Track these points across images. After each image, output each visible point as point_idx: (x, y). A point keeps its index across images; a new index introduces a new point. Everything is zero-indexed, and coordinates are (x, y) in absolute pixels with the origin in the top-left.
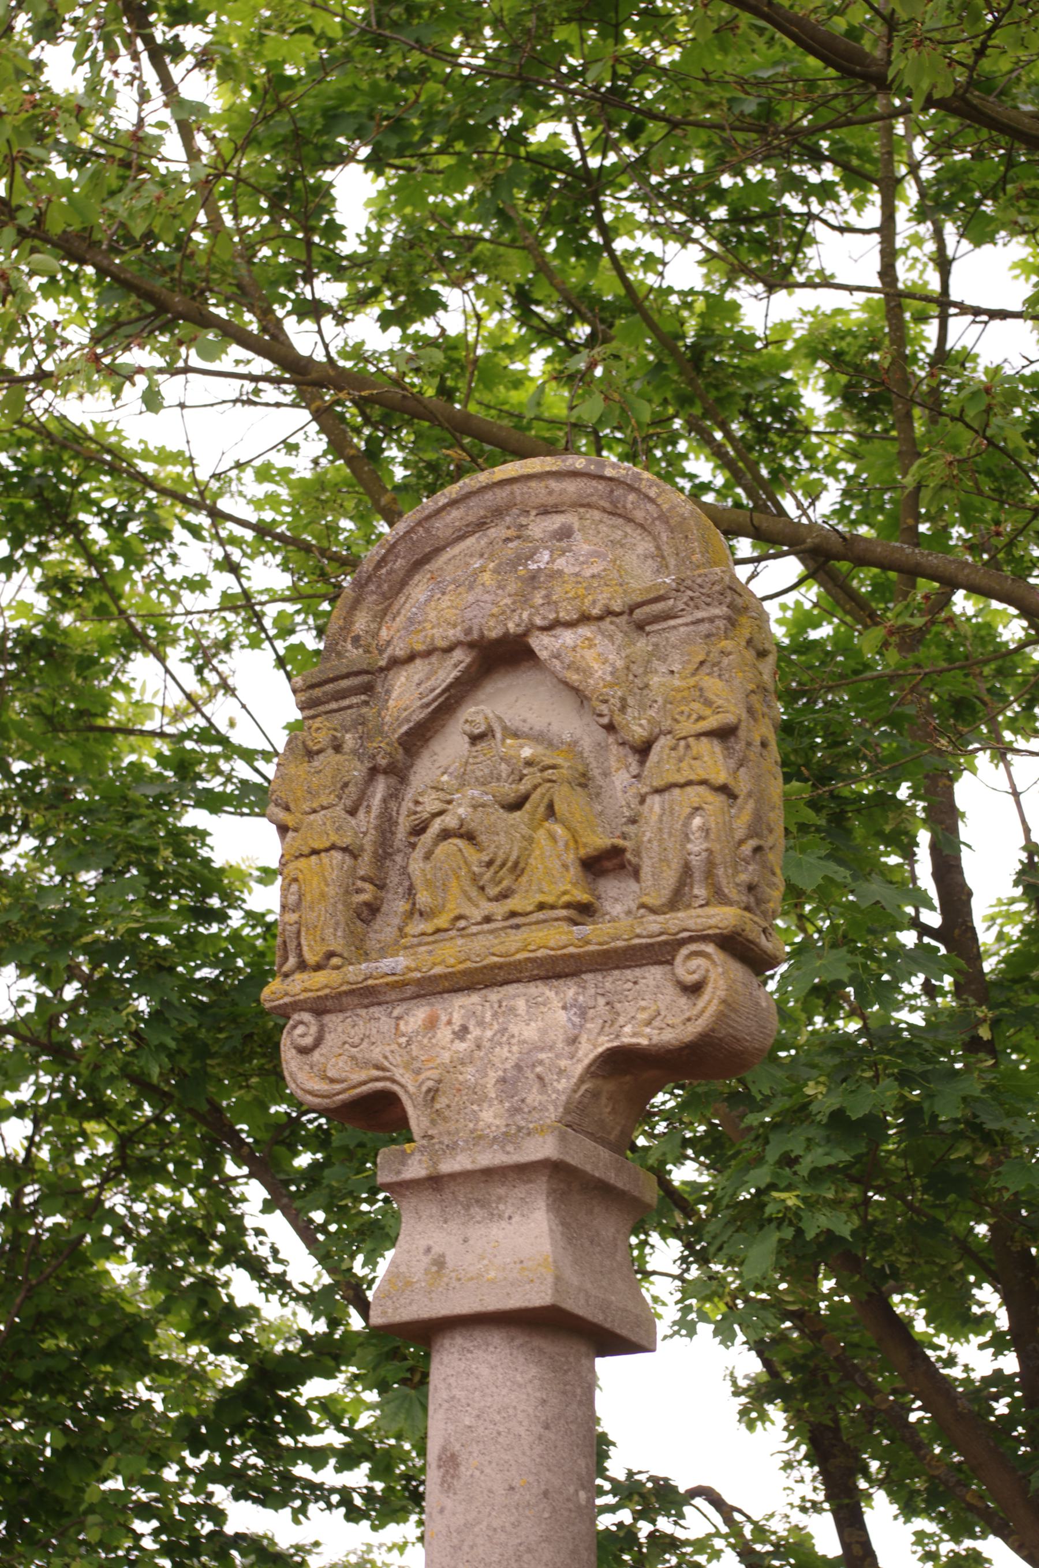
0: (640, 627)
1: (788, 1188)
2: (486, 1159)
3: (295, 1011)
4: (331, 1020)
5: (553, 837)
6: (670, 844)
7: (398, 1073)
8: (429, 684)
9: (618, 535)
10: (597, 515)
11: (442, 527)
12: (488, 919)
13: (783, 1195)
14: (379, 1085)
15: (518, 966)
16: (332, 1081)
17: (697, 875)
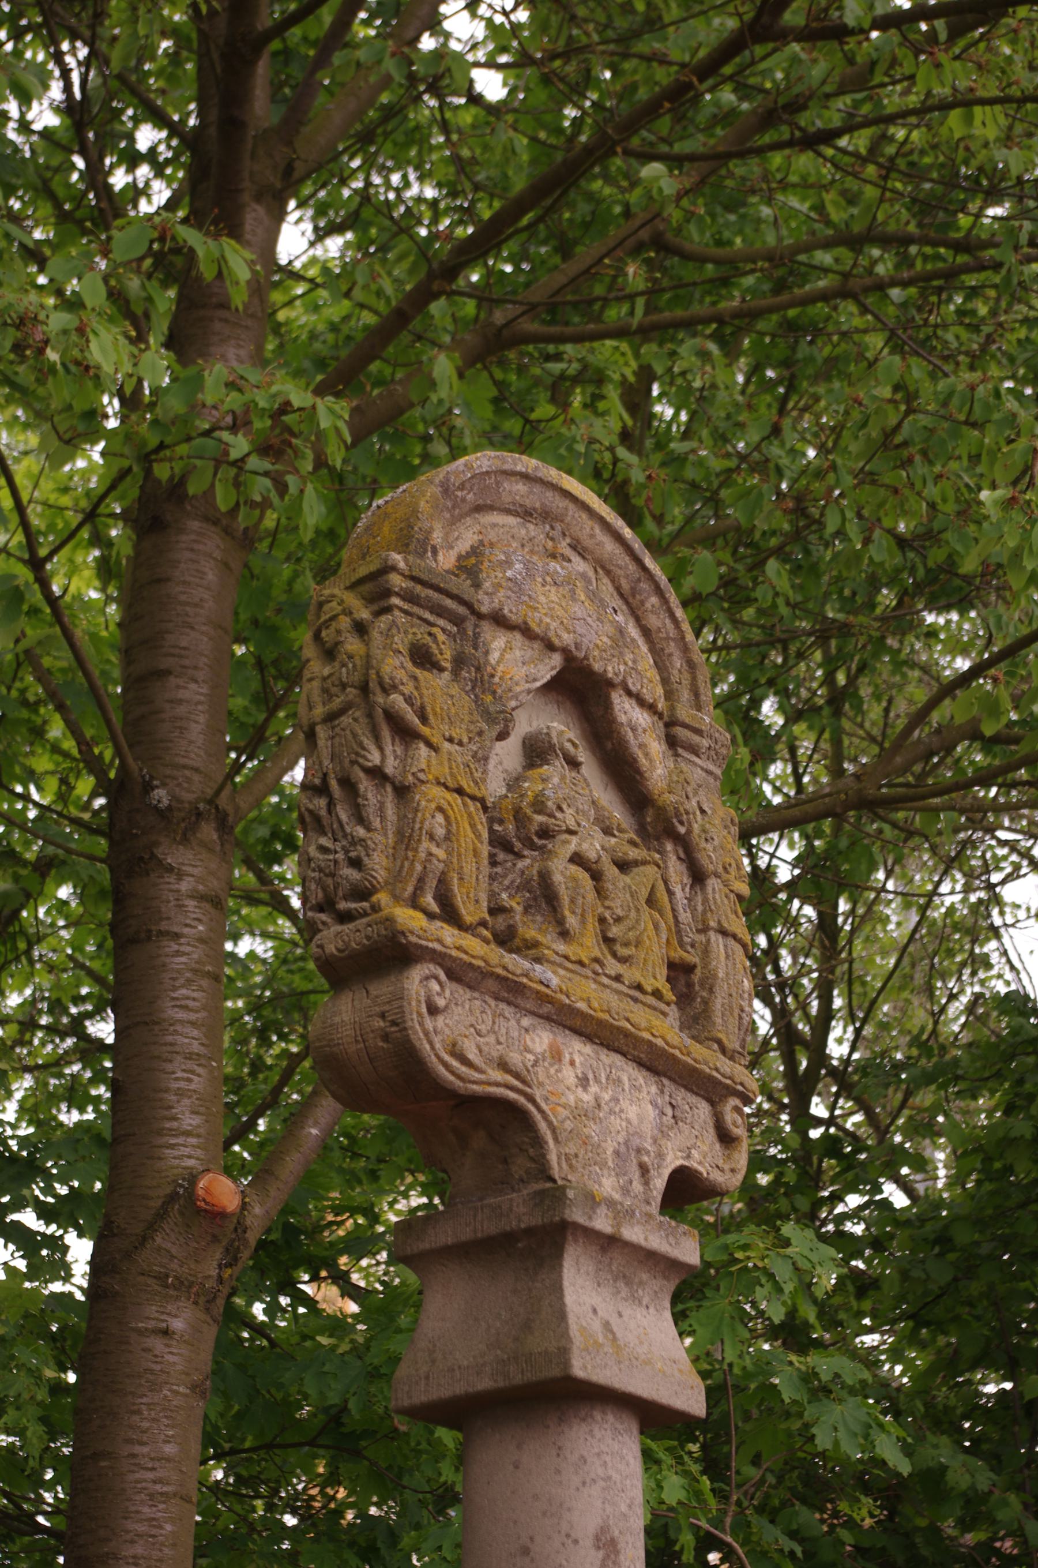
3: (433, 960)
12: (618, 978)
14: (512, 1095)
15: (638, 1041)
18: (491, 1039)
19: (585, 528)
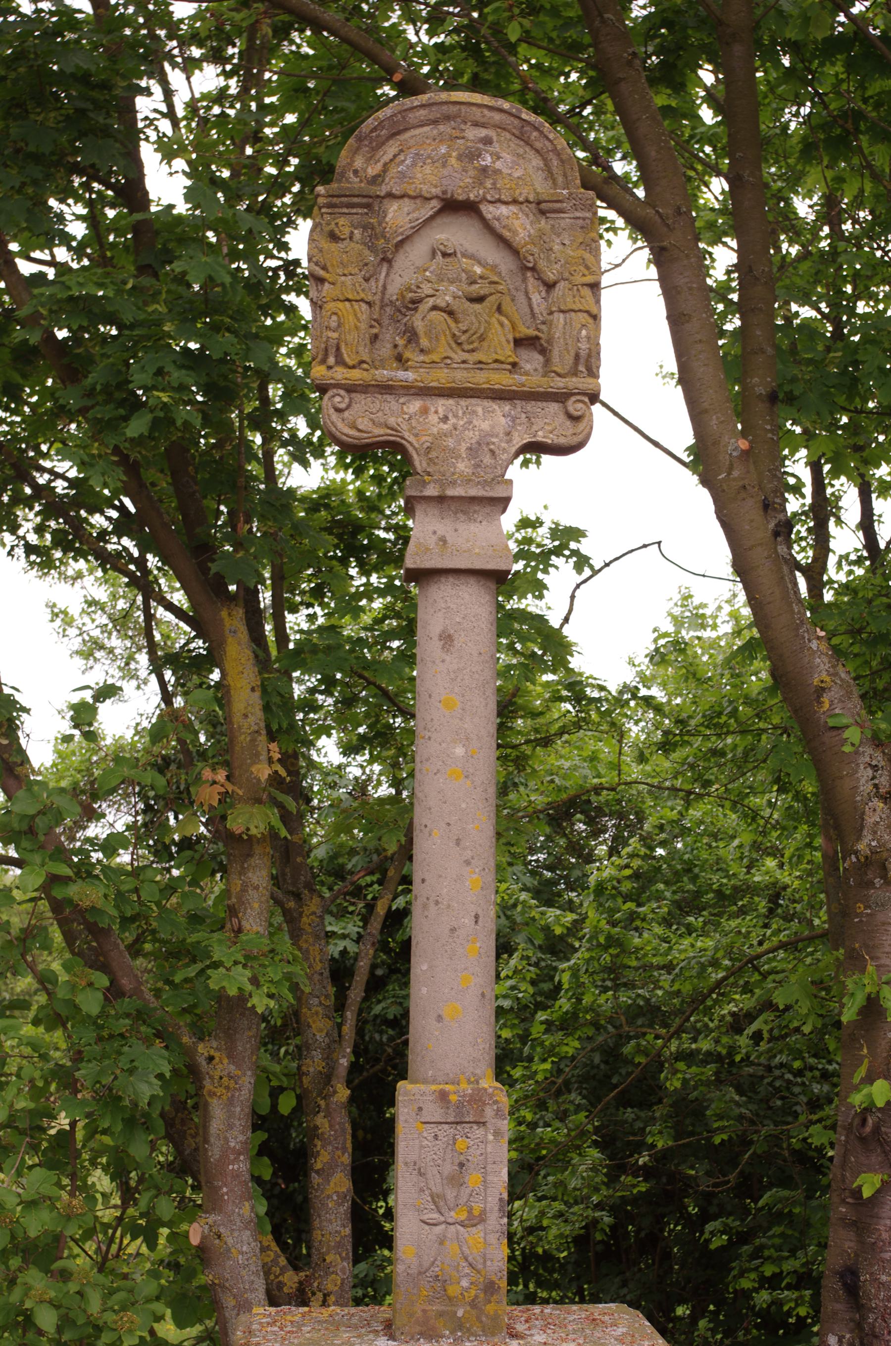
0: (543, 212)
1: (163, 390)
2: (473, 492)
4: (357, 396)
5: (502, 325)
6: (570, 342)
7: (406, 435)
8: (415, 215)
9: (521, 151)
10: (508, 136)
11: (412, 117)
12: (464, 362)
13: (161, 394)
16: (359, 430)
17: (582, 361)
18: (380, 414)
19: (477, 113)
